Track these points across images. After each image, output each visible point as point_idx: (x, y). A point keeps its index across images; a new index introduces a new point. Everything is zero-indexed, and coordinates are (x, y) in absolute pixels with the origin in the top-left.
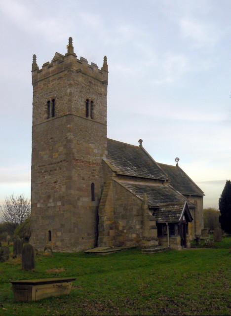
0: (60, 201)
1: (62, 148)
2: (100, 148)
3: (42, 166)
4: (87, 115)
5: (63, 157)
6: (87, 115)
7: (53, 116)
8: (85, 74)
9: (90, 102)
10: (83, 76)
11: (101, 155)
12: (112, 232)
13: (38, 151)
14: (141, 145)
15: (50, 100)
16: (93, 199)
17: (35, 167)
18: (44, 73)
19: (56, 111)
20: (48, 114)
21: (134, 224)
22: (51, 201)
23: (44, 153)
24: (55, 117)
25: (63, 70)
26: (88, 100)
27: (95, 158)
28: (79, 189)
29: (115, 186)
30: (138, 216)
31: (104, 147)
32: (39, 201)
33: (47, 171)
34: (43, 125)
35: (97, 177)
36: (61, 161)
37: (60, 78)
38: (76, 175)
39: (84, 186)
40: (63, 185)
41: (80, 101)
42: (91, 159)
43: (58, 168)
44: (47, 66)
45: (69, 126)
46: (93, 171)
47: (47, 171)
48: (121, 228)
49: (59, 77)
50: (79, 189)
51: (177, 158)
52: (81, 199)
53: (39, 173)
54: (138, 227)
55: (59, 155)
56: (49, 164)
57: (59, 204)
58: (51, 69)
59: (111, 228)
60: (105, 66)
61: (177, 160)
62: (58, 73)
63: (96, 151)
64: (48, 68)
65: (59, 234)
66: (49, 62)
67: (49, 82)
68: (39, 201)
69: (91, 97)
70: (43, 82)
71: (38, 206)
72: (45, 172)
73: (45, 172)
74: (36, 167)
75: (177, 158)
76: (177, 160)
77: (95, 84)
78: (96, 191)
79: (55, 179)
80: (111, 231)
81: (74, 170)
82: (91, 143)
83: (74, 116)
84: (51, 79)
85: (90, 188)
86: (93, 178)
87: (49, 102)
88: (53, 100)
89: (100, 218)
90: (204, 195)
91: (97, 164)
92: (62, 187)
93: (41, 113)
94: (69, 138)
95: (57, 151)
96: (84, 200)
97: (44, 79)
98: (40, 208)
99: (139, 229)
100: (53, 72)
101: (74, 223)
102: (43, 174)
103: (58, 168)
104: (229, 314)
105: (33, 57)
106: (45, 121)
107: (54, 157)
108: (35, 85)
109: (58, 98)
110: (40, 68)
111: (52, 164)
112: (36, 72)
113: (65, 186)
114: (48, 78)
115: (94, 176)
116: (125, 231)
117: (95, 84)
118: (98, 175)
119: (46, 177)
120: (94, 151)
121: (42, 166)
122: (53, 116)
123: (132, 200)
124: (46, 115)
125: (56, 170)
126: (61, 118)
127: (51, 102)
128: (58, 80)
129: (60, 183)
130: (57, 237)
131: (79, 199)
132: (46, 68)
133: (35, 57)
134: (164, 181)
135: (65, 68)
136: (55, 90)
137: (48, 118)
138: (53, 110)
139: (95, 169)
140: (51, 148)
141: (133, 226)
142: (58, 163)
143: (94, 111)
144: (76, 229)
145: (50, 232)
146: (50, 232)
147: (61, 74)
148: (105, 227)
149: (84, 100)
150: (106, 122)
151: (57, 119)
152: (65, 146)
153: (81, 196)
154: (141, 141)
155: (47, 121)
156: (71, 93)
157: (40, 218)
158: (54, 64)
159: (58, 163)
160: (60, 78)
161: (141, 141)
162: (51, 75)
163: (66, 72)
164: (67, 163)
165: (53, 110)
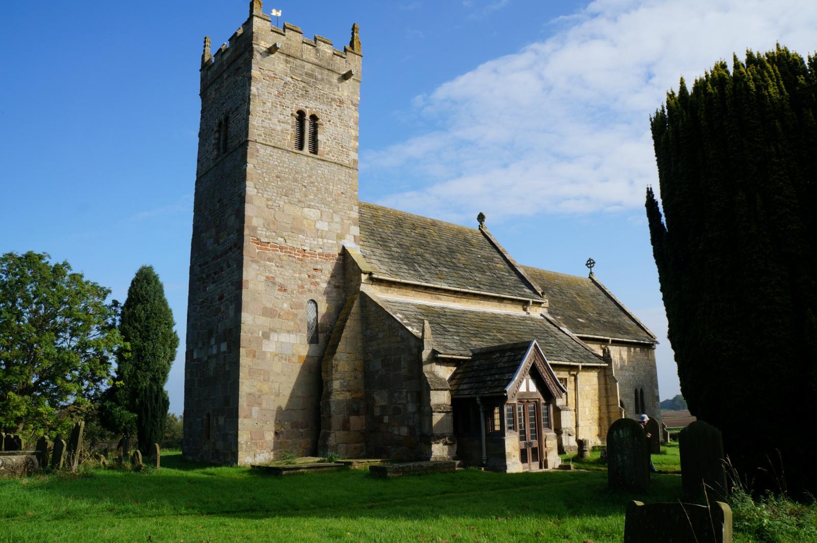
0: (225, 341)
4: (301, 146)
11: (340, 237)
12: (356, 422)
20: (219, 149)
21: (404, 401)
26: (301, 114)
31: (349, 218)
39: (285, 305)
42: (308, 243)
46: (314, 273)
48: (377, 412)
54: (411, 408)
59: (356, 413)
61: (590, 263)
63: (323, 226)
69: (310, 107)
75: (590, 260)
76: (590, 263)
77: (322, 80)
80: (353, 419)
81: (255, 266)
82: (309, 207)
83: (258, 146)
89: (324, 384)
90: (657, 343)
99: (414, 413)
116: (386, 419)
117: (322, 80)
131: (266, 336)
139: (319, 267)
141: (401, 406)
148: (333, 408)
150: (201, 119)
153: (273, 330)
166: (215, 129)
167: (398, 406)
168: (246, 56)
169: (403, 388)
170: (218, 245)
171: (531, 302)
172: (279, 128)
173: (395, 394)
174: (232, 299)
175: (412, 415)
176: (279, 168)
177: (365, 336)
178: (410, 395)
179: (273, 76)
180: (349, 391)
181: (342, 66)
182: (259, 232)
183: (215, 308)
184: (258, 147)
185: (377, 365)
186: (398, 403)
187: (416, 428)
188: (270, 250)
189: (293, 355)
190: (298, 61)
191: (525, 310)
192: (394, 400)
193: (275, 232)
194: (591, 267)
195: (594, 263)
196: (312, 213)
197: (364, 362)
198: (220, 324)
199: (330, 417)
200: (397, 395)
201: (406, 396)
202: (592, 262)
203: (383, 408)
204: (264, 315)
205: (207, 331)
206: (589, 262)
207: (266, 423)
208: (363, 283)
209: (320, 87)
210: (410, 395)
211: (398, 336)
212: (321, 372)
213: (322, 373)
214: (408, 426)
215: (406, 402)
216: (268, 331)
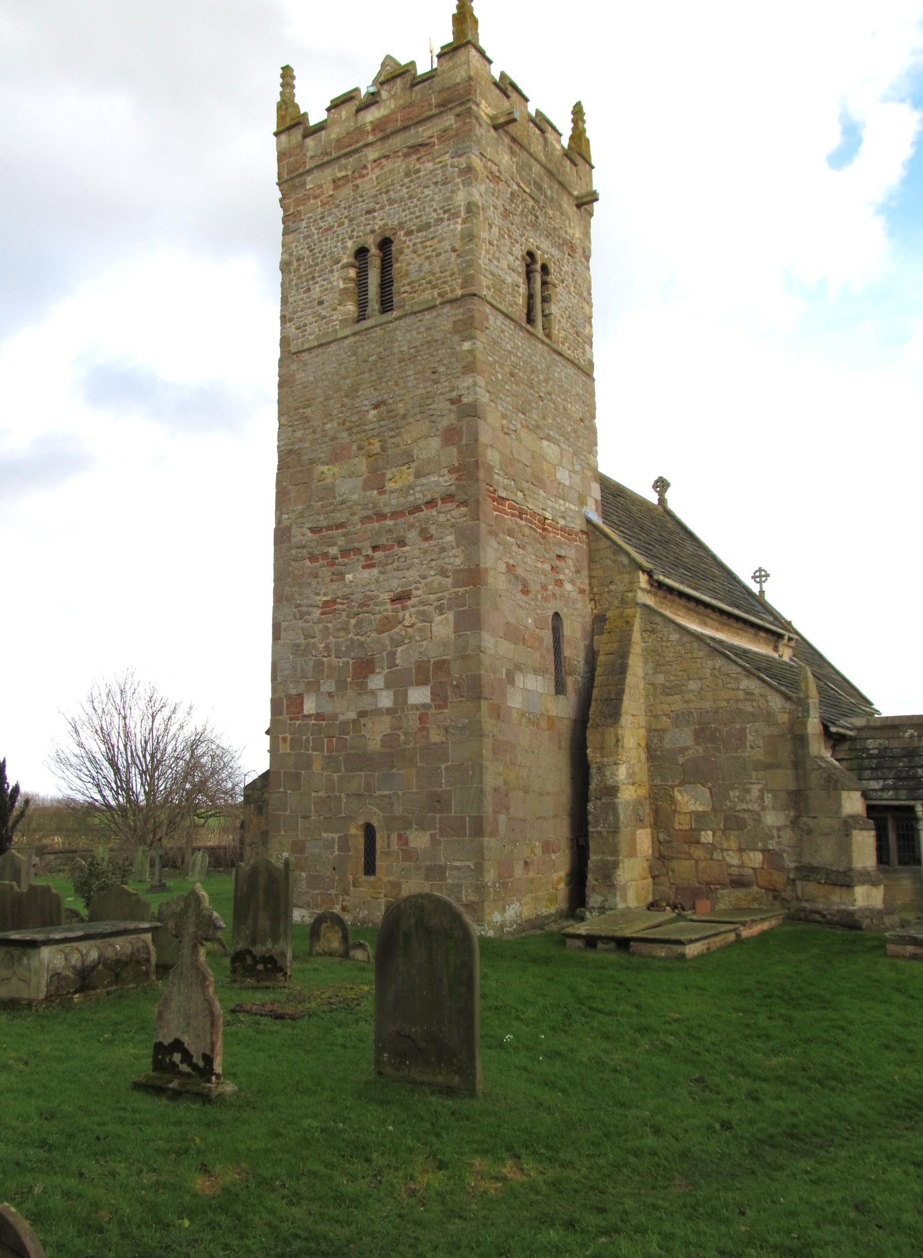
1: (435, 443)
2: (578, 468)
3: (329, 528)
5: (442, 481)
6: (530, 320)
7: (386, 305)
8: (522, 147)
9: (538, 267)
10: (513, 153)
13: (312, 462)
14: (662, 501)
15: (371, 243)
16: (560, 688)
17: (295, 531)
18: (334, 133)
19: (400, 287)
20: (362, 305)
21: (756, 807)
22: (376, 682)
23: (336, 469)
24: (395, 314)
25: (434, 111)
27: (562, 505)
28: (513, 634)
29: (653, 631)
30: (768, 766)
32: (313, 686)
33: (358, 551)
34: (333, 347)
35: (568, 587)
36: (431, 503)
37: (415, 148)
38: (503, 567)
40: (441, 609)
41: (506, 249)
43: (412, 535)
44: (352, 106)
45: (466, 346)
47: (358, 551)
49: (412, 142)
50: (513, 634)
51: (760, 570)
52: (519, 679)
53: (313, 558)
55: (418, 475)
56: (366, 520)
57: (419, 695)
58: (372, 115)
60: (578, 136)
62: (405, 128)
64: (358, 111)
65: (419, 840)
66: (357, 90)
67: (361, 171)
68: (313, 686)
69: (546, 250)
70: (329, 174)
71: (310, 706)
72: (345, 553)
73: (345, 553)
74: (302, 534)
75: (760, 570)
78: (567, 652)
79: (396, 585)
82: (548, 438)
84: (372, 154)
85: (548, 635)
86: (557, 590)
87: (361, 253)
88: (385, 244)
89: (593, 771)
91: (567, 532)
92: (438, 619)
93: (321, 303)
94: (465, 400)
95: (408, 458)
96: (530, 686)
97: (338, 158)
98: (319, 716)
100: (378, 126)
101: (496, 790)
102: (332, 562)
103: (412, 535)
104: (32, 1255)
105: (283, 76)
106: (348, 331)
107: (390, 486)
108: (294, 188)
109: (409, 233)
110: (316, 116)
111: (381, 516)
112: (298, 133)
113: (450, 616)
114: (356, 151)
115: (559, 583)
118: (572, 582)
119: (349, 577)
120: (559, 476)
121: (329, 528)
122: (386, 305)
123: (741, 695)
124: (351, 308)
125: (402, 543)
126: (428, 316)
127: (374, 250)
128: (406, 155)
129: (422, 603)
130: (409, 854)
132: (344, 112)
133: (287, 74)
134: (780, 636)
135: (438, 105)
136: (391, 202)
137: (362, 316)
138: (386, 284)
139: (563, 553)
140: (376, 447)
142: (416, 509)
143: (554, 309)
144: (502, 818)
145: (369, 831)
146: (369, 831)
147: (424, 132)
149: (519, 251)
151: (408, 320)
152: (450, 436)
153: (518, 667)
154: (661, 485)
155: (355, 334)
156: (471, 208)
157: (317, 767)
158: (384, 94)
159: (416, 509)
160: (415, 148)
161: (661, 485)
162: (371, 138)
163: (449, 120)
164: (463, 509)
165: (386, 284)
166: (345, 261)
167: (738, 814)
168: (447, 124)
169: (751, 783)
170: (380, 493)
171: (786, 637)
172: (509, 280)
173: (731, 794)
174: (445, 601)
175: (775, 833)
176: (513, 358)
177: (652, 684)
178: (770, 795)
179: (497, 174)
180: (633, 784)
181: (457, 184)
182: (496, 477)
183: (378, 616)
184: (488, 311)
185: (684, 737)
186: (739, 808)
187: (785, 855)
188: (507, 514)
189: (542, 714)
190: (525, 154)
191: (776, 649)
192: (728, 803)
193: (514, 480)
194: (760, 583)
195: (767, 575)
196: (550, 450)
197: (649, 730)
198: (399, 649)
199: (615, 830)
200: (737, 794)
201: (761, 798)
202: (763, 573)
203: (698, 816)
204: (506, 637)
205: (351, 662)
206: (758, 574)
207: (515, 846)
208: (643, 590)
209: (550, 212)
210: (770, 795)
211: (738, 689)
212: (585, 747)
213: (588, 751)
214: (765, 851)
215: (759, 809)
216: (511, 668)
